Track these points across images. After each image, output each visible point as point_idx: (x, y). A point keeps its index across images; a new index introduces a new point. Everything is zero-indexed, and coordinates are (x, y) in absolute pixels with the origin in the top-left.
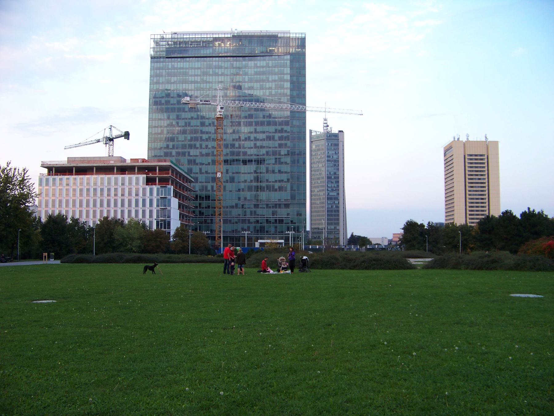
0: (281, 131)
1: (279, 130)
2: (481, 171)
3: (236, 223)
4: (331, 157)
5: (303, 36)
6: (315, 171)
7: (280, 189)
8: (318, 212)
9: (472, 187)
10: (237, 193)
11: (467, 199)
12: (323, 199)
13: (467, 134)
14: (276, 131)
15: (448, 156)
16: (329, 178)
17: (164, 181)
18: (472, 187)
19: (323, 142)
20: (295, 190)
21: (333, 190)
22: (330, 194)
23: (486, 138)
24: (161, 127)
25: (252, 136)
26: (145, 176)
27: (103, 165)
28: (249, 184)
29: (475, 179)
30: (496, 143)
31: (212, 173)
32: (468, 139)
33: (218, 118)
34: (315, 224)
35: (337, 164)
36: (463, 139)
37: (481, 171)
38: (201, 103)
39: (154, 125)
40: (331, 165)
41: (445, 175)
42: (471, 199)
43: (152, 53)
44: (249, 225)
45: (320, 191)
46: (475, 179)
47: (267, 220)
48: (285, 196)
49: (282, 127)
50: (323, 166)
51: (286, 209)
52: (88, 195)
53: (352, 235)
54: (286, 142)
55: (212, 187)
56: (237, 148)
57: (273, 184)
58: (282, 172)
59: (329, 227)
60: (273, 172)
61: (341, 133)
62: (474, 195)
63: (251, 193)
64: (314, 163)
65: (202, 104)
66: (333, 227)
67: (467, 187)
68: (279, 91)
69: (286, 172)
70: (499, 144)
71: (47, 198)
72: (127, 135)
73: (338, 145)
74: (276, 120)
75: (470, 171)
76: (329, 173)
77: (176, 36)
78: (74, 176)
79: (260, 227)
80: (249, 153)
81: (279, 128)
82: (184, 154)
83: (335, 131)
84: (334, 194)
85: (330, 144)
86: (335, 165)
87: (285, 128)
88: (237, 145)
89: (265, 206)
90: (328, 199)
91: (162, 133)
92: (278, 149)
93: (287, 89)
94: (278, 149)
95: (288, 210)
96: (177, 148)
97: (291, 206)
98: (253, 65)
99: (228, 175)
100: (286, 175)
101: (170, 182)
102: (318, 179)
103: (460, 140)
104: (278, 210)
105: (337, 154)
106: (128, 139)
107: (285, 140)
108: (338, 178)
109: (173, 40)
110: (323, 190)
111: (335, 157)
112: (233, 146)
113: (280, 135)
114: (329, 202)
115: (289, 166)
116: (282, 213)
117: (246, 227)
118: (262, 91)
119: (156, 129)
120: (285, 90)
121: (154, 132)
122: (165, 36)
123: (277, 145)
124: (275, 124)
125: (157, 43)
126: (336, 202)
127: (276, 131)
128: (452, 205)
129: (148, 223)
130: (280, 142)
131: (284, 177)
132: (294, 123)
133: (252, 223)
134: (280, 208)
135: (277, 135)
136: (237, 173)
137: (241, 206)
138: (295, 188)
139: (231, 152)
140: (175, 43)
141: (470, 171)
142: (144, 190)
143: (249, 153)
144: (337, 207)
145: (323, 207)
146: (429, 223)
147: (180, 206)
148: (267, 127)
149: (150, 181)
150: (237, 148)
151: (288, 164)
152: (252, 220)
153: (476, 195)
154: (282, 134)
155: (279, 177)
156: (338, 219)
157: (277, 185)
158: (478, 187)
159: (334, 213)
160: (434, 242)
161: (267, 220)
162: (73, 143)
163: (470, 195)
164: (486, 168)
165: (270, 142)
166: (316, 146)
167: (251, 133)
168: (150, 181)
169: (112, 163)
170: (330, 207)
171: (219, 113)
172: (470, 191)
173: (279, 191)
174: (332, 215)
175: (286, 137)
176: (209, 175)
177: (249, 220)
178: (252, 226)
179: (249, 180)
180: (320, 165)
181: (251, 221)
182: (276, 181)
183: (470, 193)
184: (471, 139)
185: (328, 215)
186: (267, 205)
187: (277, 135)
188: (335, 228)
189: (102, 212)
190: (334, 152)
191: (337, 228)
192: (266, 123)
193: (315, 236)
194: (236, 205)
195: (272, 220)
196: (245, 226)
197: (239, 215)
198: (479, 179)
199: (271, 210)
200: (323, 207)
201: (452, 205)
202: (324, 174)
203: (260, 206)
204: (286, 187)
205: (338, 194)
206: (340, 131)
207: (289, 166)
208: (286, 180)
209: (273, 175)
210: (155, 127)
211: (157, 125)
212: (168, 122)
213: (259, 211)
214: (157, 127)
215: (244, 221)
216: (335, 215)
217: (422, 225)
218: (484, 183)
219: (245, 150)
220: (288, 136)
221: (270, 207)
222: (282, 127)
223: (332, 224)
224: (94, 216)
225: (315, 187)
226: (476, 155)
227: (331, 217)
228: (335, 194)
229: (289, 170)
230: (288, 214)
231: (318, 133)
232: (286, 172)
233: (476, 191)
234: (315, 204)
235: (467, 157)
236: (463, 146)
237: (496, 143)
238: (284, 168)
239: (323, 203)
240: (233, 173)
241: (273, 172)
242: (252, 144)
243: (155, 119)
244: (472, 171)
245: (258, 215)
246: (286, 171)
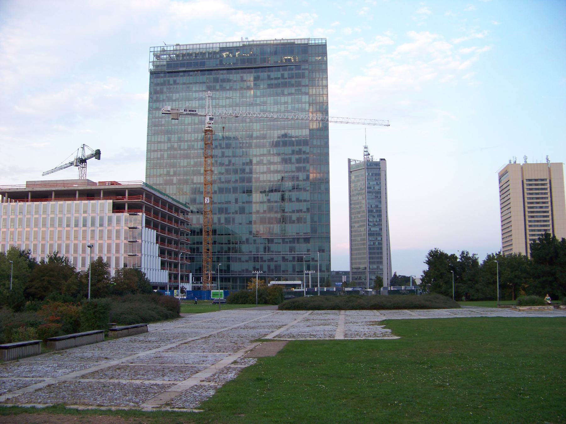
0: (299, 152)
1: (297, 151)
2: (542, 198)
3: (247, 261)
4: (372, 188)
5: (324, 41)
6: (355, 204)
7: (299, 220)
8: (359, 249)
9: (532, 217)
10: (248, 226)
11: (528, 231)
12: (364, 235)
13: (525, 156)
14: (293, 152)
15: (503, 182)
16: (370, 211)
17: (134, 209)
18: (532, 217)
19: (363, 172)
20: (316, 222)
22: (372, 229)
23: (547, 159)
24: (161, 150)
25: (265, 160)
26: (111, 201)
27: (63, 188)
28: (262, 215)
29: (536, 207)
30: (560, 165)
31: (219, 203)
32: (526, 162)
33: (206, 130)
34: (356, 263)
35: (379, 196)
36: (521, 162)
37: (542, 198)
38: (185, 113)
39: (152, 149)
40: (373, 197)
41: (501, 204)
42: (532, 230)
43: (152, 67)
44: (262, 263)
45: (361, 226)
46: (536, 207)
47: (283, 258)
48: (304, 229)
49: (300, 147)
50: (363, 199)
51: (305, 245)
52: (110, 232)
53: (395, 275)
54: (304, 165)
55: (219, 219)
56: (247, 173)
57: (290, 214)
58: (301, 201)
59: (371, 267)
60: (290, 200)
61: (383, 161)
62: (535, 226)
63: (265, 226)
64: (354, 195)
65: (187, 114)
66: (375, 266)
67: (527, 217)
68: (297, 106)
69: (305, 201)
70: (564, 165)
71: (109, 242)
72: (97, 154)
73: (379, 175)
74: (293, 139)
75: (530, 198)
76: (370, 207)
77: (178, 48)
78: (29, 203)
79: (276, 267)
80: (261, 179)
81: (297, 148)
82: (186, 182)
83: (376, 159)
84: (377, 229)
85: (370, 174)
86: (376, 197)
87: (304, 148)
88: (247, 170)
89: (281, 241)
90: (370, 235)
91: (162, 157)
92: (296, 174)
93: (305, 103)
94: (296, 174)
95: (309, 246)
96: (179, 175)
97: (311, 240)
98: (266, 77)
99: (237, 205)
100: (305, 203)
101: (144, 209)
102: (359, 213)
103: (517, 163)
104: (296, 245)
105: (379, 184)
106: (99, 159)
107: (304, 163)
108: (380, 211)
109: (175, 52)
110: (364, 225)
111: (377, 188)
112: (243, 171)
113: (297, 156)
114: (370, 239)
115: (308, 193)
116: (301, 249)
117: (258, 266)
118: (276, 106)
119: (156, 153)
120: (304, 105)
121: (152, 157)
122: (166, 49)
123: (294, 169)
124: (292, 144)
125: (157, 56)
126: (379, 238)
127: (293, 152)
128: (510, 239)
129: (71, 259)
130: (297, 165)
131: (303, 206)
132: (315, 143)
133: (265, 261)
134: (298, 242)
135: (294, 158)
136: (247, 202)
137: (252, 242)
138: (316, 219)
139: (240, 178)
140: (177, 56)
141: (530, 198)
142: (110, 219)
143: (261, 179)
144: (380, 244)
145: (364, 244)
146: (463, 253)
147: (160, 240)
148: (283, 148)
149: (118, 208)
150: (247, 173)
151: (308, 191)
152: (266, 257)
153: (537, 226)
154: (300, 156)
155: (296, 206)
156: (381, 258)
157: (294, 216)
158: (540, 216)
159: (376, 251)
160: (470, 280)
161: (283, 258)
162: (50, 169)
163: (530, 226)
164: (549, 194)
165: (286, 165)
166: (356, 177)
167: (263, 155)
168: (118, 208)
169: (76, 187)
170: (372, 243)
171: (207, 125)
172: (530, 221)
173: (298, 223)
174: (374, 253)
175: (304, 159)
176: (215, 205)
177: (262, 258)
178: (265, 265)
179: (262, 211)
180: (360, 198)
181: (264, 259)
182: (293, 212)
183: (530, 224)
184: (529, 161)
185: (370, 253)
186: (283, 239)
187: (294, 158)
188: (378, 268)
189: (51, 246)
190: (375, 183)
191: (381, 267)
192: (281, 144)
193: (356, 276)
194: (247, 240)
195: (290, 257)
196: (258, 265)
197: (251, 252)
198: (541, 207)
199: (288, 245)
200: (364, 244)
201: (510, 239)
202: (364, 207)
203: (275, 241)
204: (305, 219)
205: (381, 229)
206: (381, 159)
207: (308, 193)
208: (305, 210)
209: (291, 204)
210: (154, 151)
211: (156, 149)
212: (169, 145)
213: (273, 247)
214: (157, 151)
215: (256, 259)
216: (378, 253)
217: (453, 257)
218: (547, 212)
219: (258, 176)
220: (308, 158)
221: (287, 243)
222: (300, 147)
224: (43, 251)
225: (355, 222)
226: (536, 180)
227: (373, 256)
228: (378, 229)
229: (308, 199)
230: (308, 250)
231: (357, 162)
232: (305, 201)
233: (538, 221)
234: (355, 240)
235: (525, 182)
236: (520, 169)
237: (560, 165)
238: (304, 195)
239: (364, 240)
240: (243, 203)
241: (290, 200)
242: (265, 168)
243: (154, 143)
244: (533, 198)
245: (273, 252)
246: (305, 199)
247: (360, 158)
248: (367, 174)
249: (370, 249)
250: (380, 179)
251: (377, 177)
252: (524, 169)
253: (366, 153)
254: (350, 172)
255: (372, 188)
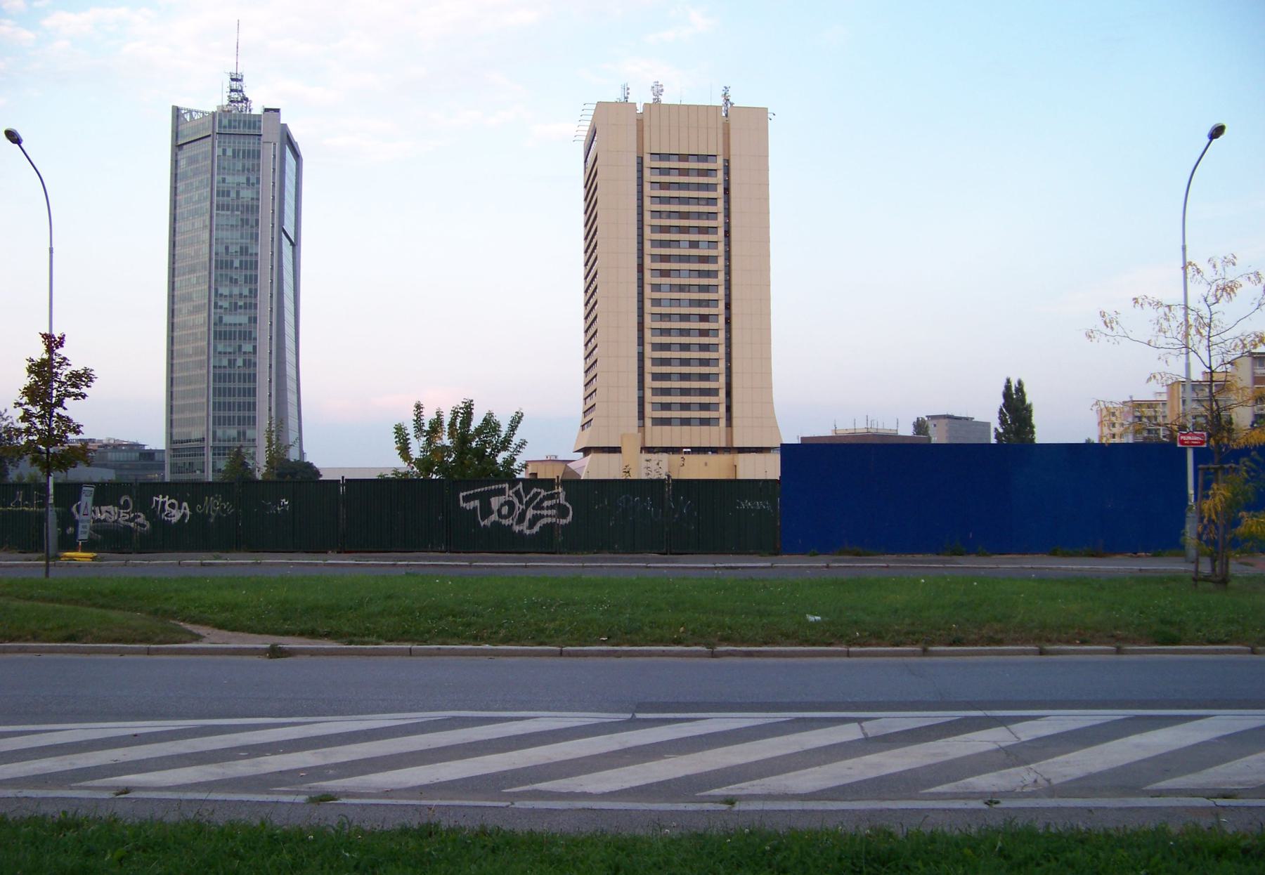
2: (699, 215)
4: (233, 195)
21: (235, 307)
22: (228, 319)
30: (759, 117)
35: (252, 219)
59: (219, 433)
76: (222, 249)
85: (229, 152)
86: (245, 222)
90: (219, 336)
111: (247, 194)
114: (220, 348)
126: (247, 347)
144: (249, 364)
166: (192, 160)
170: (225, 362)
174: (231, 392)
184: (664, 100)
188: (242, 435)
190: (243, 179)
191: (249, 433)
198: (694, 244)
205: (253, 320)
206: (267, 110)
223: (229, 421)
226: (683, 157)
228: (243, 319)
235: (647, 162)
237: (759, 117)
247: (208, 99)
248: (218, 151)
249: (218, 378)
250: (256, 169)
251: (249, 163)
252: (646, 123)
253: (235, 95)
254: (177, 147)
255: (233, 195)
